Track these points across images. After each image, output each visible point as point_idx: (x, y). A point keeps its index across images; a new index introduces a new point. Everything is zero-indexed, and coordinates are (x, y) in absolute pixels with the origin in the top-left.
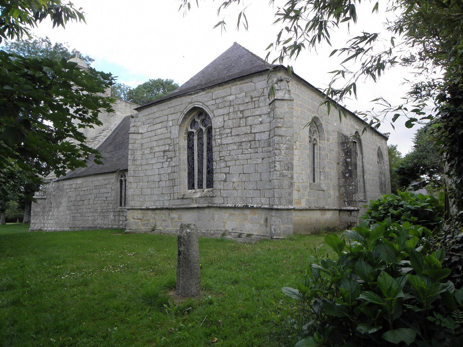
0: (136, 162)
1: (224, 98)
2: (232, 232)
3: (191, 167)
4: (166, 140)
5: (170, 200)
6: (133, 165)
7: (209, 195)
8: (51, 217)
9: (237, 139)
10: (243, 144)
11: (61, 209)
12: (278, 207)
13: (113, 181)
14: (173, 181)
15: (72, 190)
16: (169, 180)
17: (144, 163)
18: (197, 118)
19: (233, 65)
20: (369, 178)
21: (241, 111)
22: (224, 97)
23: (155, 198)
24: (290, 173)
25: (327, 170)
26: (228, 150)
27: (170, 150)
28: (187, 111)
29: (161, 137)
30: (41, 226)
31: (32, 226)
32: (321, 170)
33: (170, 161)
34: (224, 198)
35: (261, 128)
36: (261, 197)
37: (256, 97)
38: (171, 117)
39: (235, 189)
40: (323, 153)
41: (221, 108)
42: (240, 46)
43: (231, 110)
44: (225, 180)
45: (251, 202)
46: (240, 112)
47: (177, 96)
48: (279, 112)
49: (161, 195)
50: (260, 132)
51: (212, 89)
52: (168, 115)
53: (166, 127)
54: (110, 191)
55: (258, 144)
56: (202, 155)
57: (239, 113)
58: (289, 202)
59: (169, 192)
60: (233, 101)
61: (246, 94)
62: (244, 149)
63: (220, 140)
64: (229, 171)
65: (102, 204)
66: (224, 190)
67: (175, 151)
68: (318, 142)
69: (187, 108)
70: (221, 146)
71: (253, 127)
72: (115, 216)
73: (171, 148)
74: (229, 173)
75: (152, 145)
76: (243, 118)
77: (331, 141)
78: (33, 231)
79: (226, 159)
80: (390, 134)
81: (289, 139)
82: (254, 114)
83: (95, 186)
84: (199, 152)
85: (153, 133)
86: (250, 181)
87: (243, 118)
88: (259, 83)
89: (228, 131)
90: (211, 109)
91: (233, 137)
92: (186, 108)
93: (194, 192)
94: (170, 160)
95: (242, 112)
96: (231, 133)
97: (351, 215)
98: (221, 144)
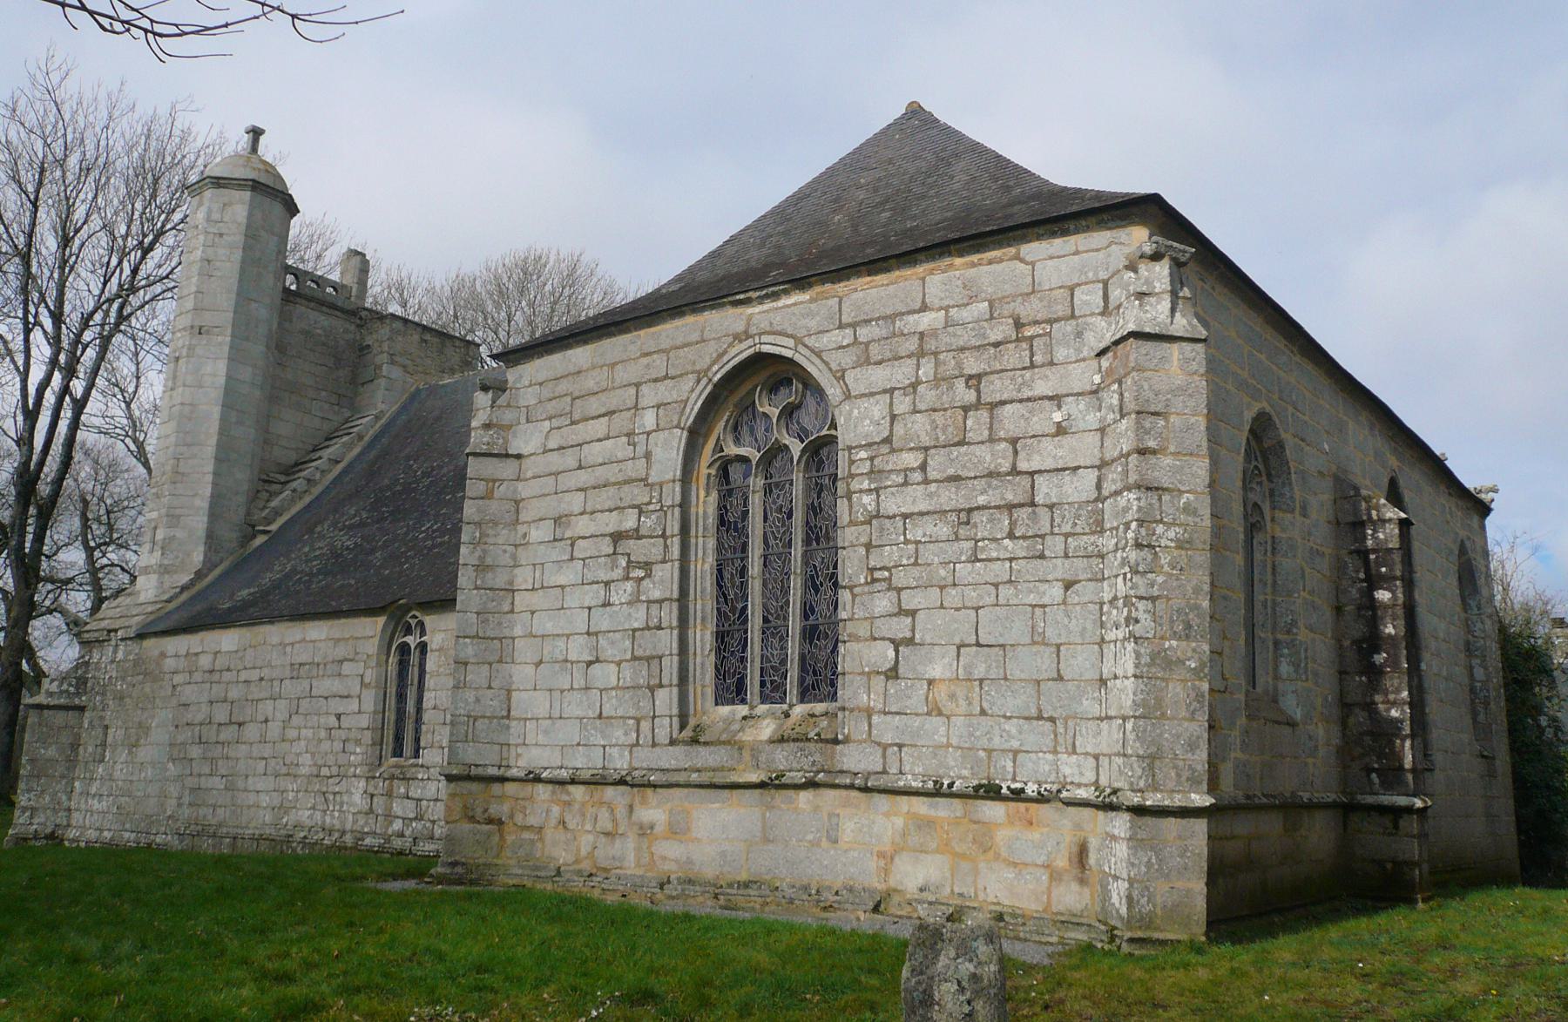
0: (490, 575)
1: (894, 323)
2: (920, 902)
3: (733, 610)
4: (626, 488)
5: (637, 744)
6: (476, 588)
7: (818, 734)
8: (102, 785)
9: (949, 497)
10: (976, 517)
11: (144, 754)
12: (1144, 799)
13: (372, 647)
14: (655, 662)
15: (197, 677)
16: (634, 658)
17: (526, 581)
18: (766, 401)
19: (917, 189)
20: (1435, 669)
21: (971, 377)
22: (897, 315)
23: (569, 732)
24: (1194, 650)
25: (1303, 635)
26: (906, 542)
27: (643, 532)
28: (724, 371)
29: (602, 473)
30: (58, 821)
31: (21, 821)
32: (1279, 636)
33: (642, 579)
34: (885, 747)
35: (1060, 453)
36: (1055, 752)
37: (1037, 323)
38: (649, 395)
39: (935, 710)
40: (1286, 564)
41: (880, 363)
42: (936, 120)
43: (926, 370)
44: (890, 670)
45: (1011, 770)
46: (967, 383)
47: (686, 305)
48: (1146, 387)
49: (598, 722)
50: (1058, 470)
51: (840, 281)
52: (637, 385)
53: (628, 435)
54: (356, 689)
55: (1049, 520)
56: (785, 558)
57: (960, 384)
58: (1188, 779)
59: (632, 713)
60: (934, 333)
61: (991, 306)
62: (983, 539)
63: (874, 496)
64: (913, 631)
65: (320, 741)
66: (886, 713)
67: (663, 536)
68: (1268, 518)
69: (725, 359)
70: (874, 522)
71: (1025, 446)
72: (372, 796)
73: (648, 522)
74: (910, 642)
75: (564, 508)
76: (977, 409)
77: (1314, 515)
78: (25, 839)
79: (900, 578)
80: (1496, 491)
81: (1188, 504)
82: (1027, 393)
83: (292, 665)
84: (772, 542)
85: (570, 460)
86: (1006, 679)
87: (977, 405)
88: (1049, 263)
89: (911, 459)
90: (834, 366)
91: (933, 487)
92: (721, 356)
93: (745, 718)
94: (641, 573)
95: (974, 380)
96: (923, 467)
97: (1396, 827)
98: (877, 516)
